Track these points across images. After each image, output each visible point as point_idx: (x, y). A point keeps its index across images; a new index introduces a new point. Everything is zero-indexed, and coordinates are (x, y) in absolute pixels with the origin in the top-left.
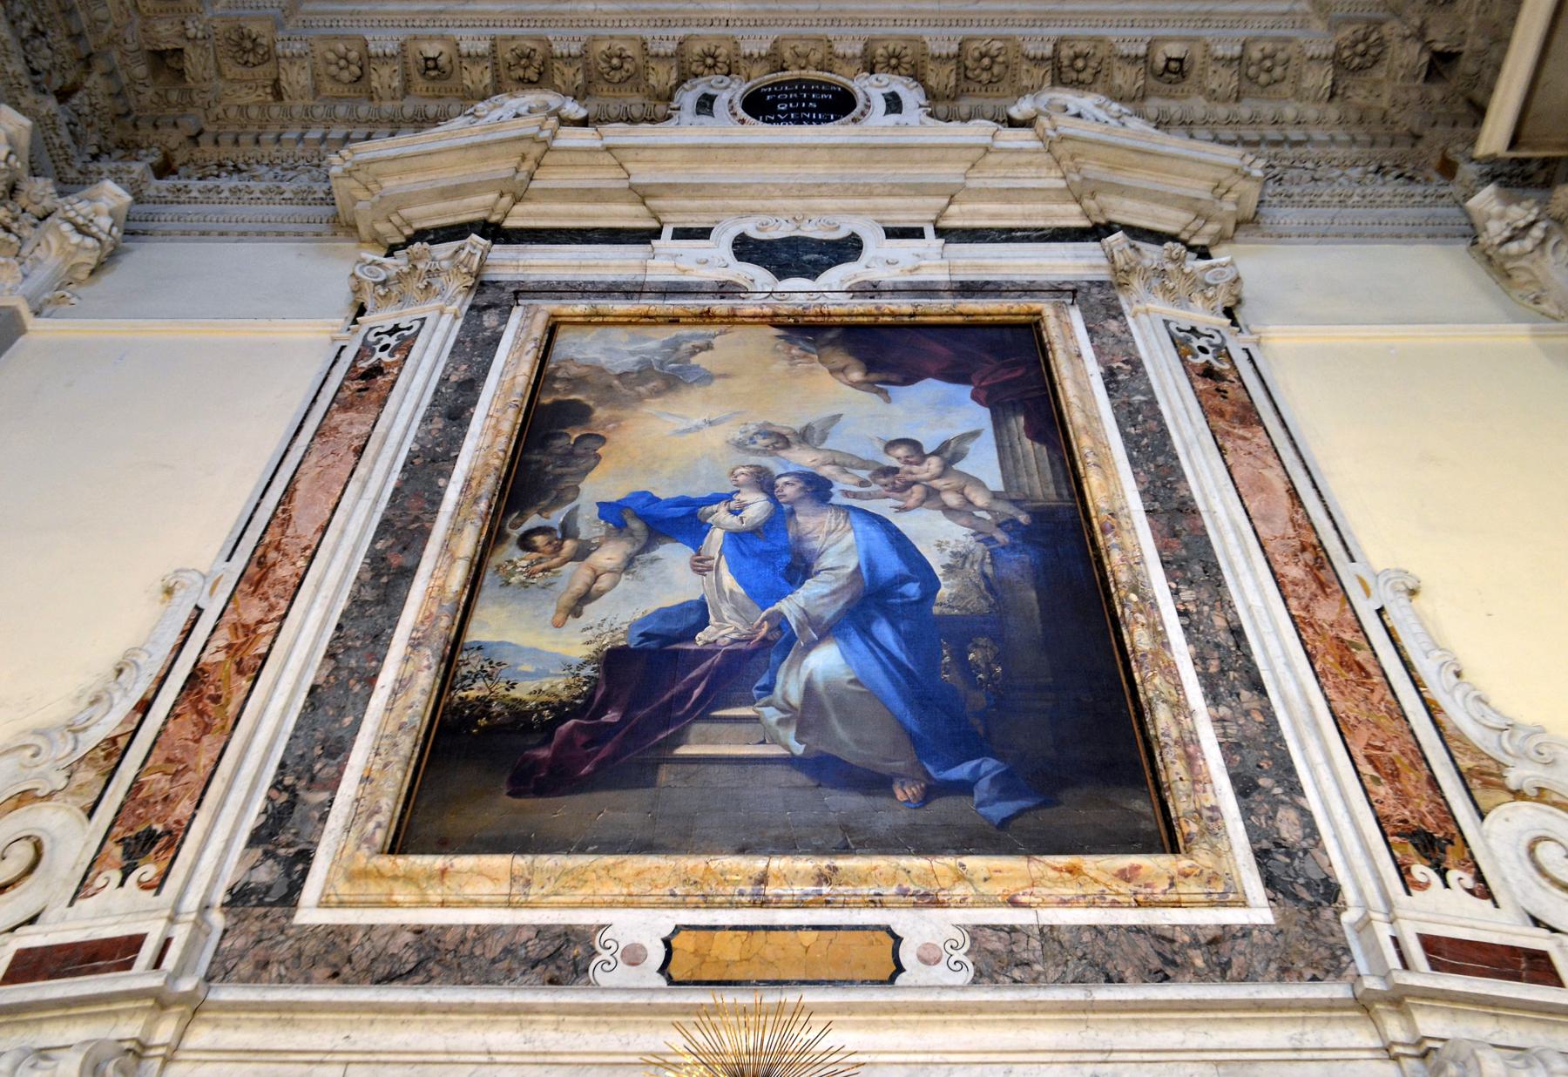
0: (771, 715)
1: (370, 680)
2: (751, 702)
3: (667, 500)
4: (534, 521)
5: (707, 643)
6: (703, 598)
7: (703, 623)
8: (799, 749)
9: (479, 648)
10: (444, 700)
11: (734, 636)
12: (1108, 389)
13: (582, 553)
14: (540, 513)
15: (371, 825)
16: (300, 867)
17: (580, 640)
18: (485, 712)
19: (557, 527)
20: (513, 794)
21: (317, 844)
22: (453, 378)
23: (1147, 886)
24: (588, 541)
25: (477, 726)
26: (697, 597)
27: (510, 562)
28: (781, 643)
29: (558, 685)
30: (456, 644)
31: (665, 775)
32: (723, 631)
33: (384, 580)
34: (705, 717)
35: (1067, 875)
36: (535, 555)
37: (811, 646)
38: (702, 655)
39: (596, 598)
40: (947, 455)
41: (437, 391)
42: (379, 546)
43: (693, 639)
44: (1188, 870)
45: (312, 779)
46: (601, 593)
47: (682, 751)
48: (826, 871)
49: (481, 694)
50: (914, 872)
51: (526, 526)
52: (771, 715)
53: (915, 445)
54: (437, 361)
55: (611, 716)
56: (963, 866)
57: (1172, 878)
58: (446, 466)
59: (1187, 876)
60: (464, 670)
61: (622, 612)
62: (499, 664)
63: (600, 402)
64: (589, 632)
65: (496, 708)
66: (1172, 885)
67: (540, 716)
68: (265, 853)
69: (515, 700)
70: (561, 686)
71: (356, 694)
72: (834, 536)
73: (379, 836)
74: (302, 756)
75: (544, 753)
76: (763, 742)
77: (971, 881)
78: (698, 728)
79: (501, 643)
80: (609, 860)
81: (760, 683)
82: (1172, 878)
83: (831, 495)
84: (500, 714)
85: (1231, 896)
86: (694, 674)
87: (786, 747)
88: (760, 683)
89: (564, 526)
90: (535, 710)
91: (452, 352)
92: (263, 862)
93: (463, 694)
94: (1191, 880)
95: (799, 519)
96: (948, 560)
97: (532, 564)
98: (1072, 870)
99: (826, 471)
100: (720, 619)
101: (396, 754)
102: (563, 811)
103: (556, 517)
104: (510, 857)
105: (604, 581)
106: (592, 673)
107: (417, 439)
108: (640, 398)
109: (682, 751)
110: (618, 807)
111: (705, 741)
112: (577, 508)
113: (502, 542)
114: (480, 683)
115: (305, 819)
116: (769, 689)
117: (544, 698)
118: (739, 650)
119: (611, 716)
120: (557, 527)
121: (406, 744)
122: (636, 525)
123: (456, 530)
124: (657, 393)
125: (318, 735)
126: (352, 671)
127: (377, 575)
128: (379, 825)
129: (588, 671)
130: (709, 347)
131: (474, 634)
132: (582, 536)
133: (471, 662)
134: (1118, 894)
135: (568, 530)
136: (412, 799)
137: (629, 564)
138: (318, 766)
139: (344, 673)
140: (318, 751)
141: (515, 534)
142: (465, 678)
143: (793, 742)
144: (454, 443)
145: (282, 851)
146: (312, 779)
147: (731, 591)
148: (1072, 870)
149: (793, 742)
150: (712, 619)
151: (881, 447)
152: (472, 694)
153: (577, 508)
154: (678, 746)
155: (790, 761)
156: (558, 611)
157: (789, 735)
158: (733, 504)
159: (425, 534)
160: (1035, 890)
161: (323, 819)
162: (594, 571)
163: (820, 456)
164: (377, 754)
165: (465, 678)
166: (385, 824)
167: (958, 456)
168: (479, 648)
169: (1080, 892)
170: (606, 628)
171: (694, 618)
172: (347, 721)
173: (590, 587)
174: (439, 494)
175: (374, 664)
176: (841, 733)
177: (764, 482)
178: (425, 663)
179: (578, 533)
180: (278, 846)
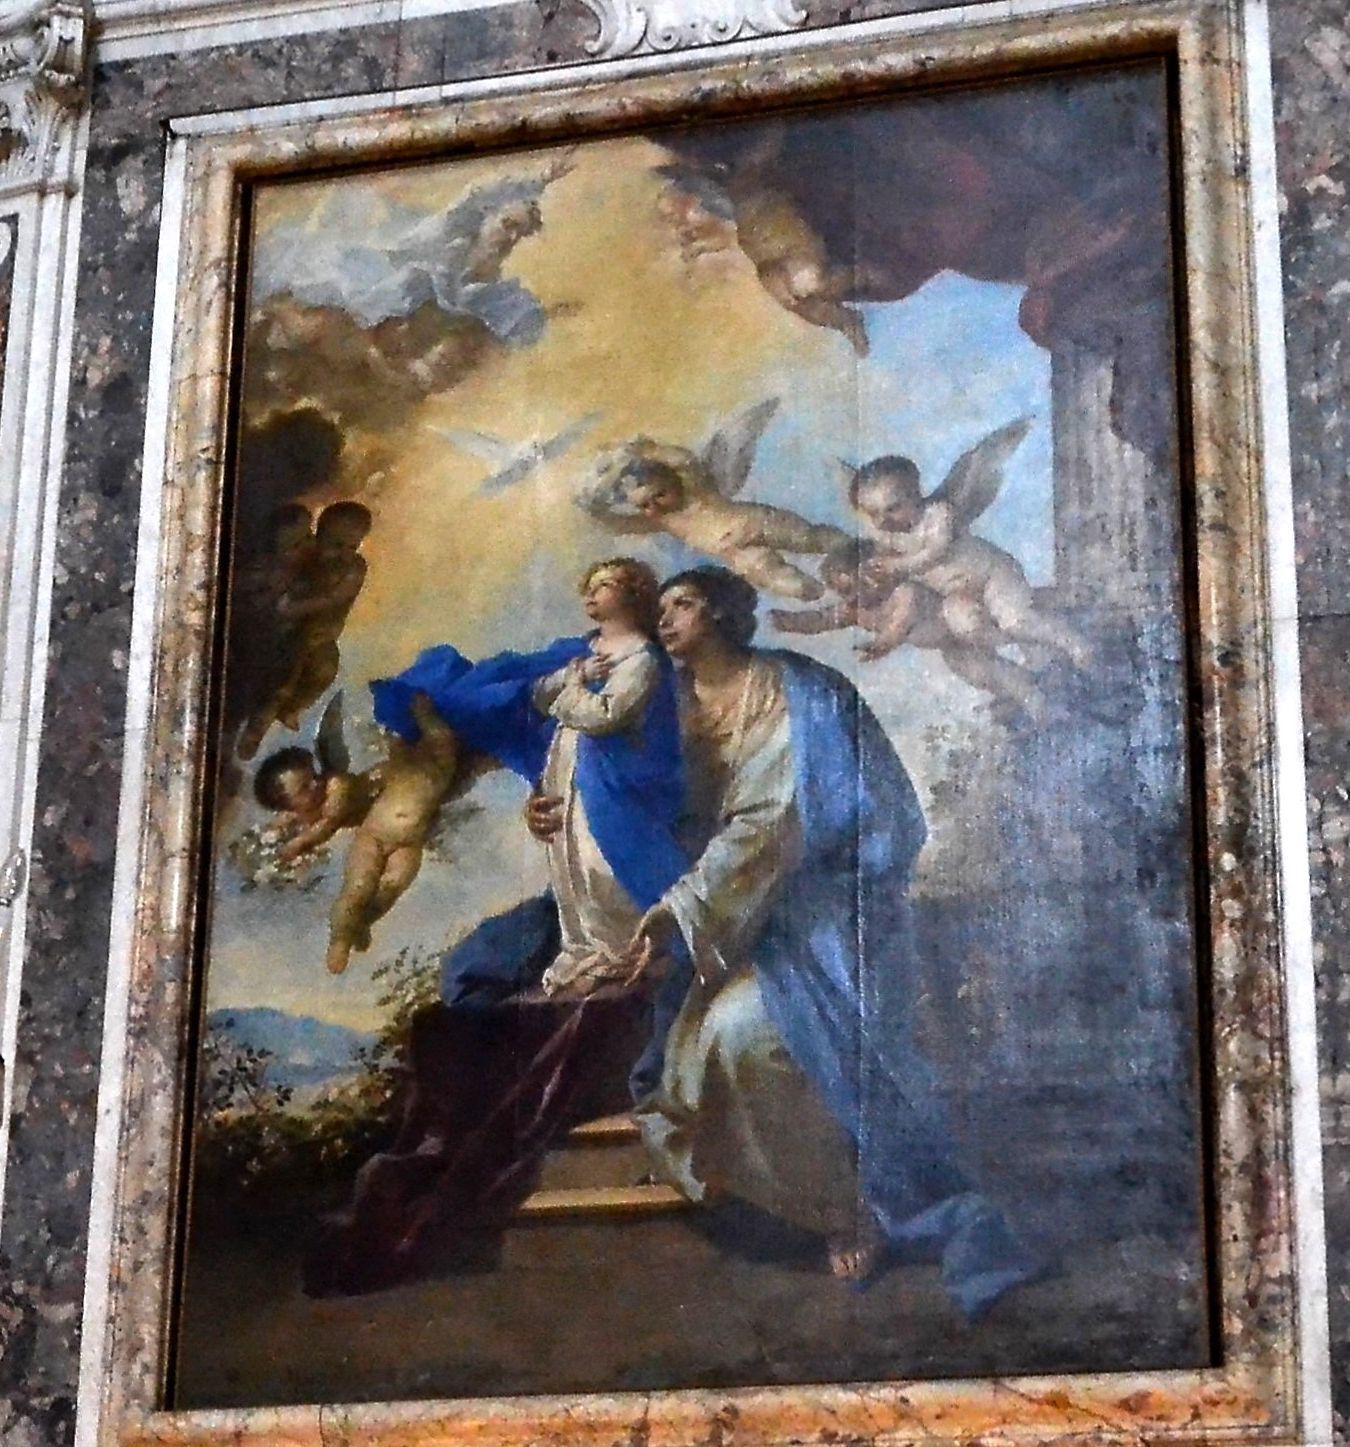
0: (657, 1128)
1: (88, 1101)
2: (622, 1106)
3: (483, 664)
4: (275, 737)
5: (560, 989)
6: (549, 893)
7: (549, 949)
8: (697, 1191)
9: (230, 1024)
10: (198, 1127)
11: (600, 971)
12: (1285, 262)
13: (356, 810)
14: (282, 718)
15: (137, 1369)
16: (62, 1426)
17: (371, 998)
18: (256, 1150)
19: (312, 748)
20: (315, 1291)
21: (76, 1388)
22: (94, 378)
23: (1160, 1418)
24: (364, 776)
25: (248, 1173)
26: (540, 892)
27: (250, 834)
28: (668, 987)
29: (347, 1086)
30: (192, 1016)
31: (513, 1248)
32: (581, 962)
33: (70, 894)
34: (568, 1143)
35: (1047, 1408)
36: (284, 817)
37: (717, 985)
38: (551, 1014)
39: (390, 903)
40: (962, 494)
41: (72, 417)
42: (49, 819)
43: (534, 983)
44: (1216, 1397)
45: (48, 1285)
46: (394, 893)
47: (535, 1203)
48: (724, 1415)
49: (244, 1113)
50: (841, 1412)
51: (263, 752)
52: (657, 1128)
53: (899, 469)
54: (56, 333)
55: (430, 1145)
56: (904, 1400)
57: (1195, 1407)
58: (114, 616)
59: (1215, 1403)
60: (214, 1069)
61: (433, 925)
62: (263, 1053)
63: (354, 414)
64: (383, 980)
65: (269, 1139)
66: (1196, 1416)
67: (332, 1152)
68: (16, 1406)
69: (292, 1121)
70: (354, 1092)
71: (75, 1130)
72: (759, 730)
73: (150, 1384)
74: (25, 1244)
75: (344, 1219)
76: (645, 1181)
77: (920, 1421)
78: (554, 1161)
79: (261, 1012)
80: (440, 1408)
81: (637, 1068)
82: (1195, 1407)
83: (752, 627)
84: (276, 1150)
85: (1277, 1430)
86: (540, 1057)
87: (679, 1188)
88: (637, 1068)
89: (323, 743)
90: (323, 1140)
91: (79, 302)
92: (16, 1421)
93: (219, 1115)
94: (1219, 1409)
95: (701, 691)
96: (943, 773)
97: (283, 839)
98: (1058, 1402)
99: (746, 563)
100: (578, 937)
101: (146, 1248)
102: (374, 1322)
103: (309, 727)
104: (315, 1408)
105: (398, 861)
106: (395, 1063)
107: (62, 554)
108: (417, 395)
109: (535, 1203)
110: (447, 1313)
111: (566, 1184)
112: (339, 695)
113: (233, 794)
114: (240, 1094)
115: (53, 1350)
116: (651, 1078)
117: (332, 1115)
118: (605, 1002)
119: (430, 1145)
120: (312, 748)
121: (156, 1226)
122: (436, 732)
123: (158, 784)
124: (449, 375)
125: (40, 1205)
126: (60, 1084)
127: (58, 886)
128: (146, 1368)
129: (388, 1060)
130: (532, 223)
131: (222, 996)
132: (355, 766)
133: (222, 1053)
134: (1120, 1431)
135: (331, 752)
136: (174, 1346)
137: (431, 826)
138: (50, 1260)
139: (49, 1089)
140: (45, 1235)
141: (249, 768)
142: (218, 1084)
143: (687, 1178)
144: (120, 551)
145: (35, 1402)
146: (48, 1285)
147: (593, 872)
148: (1058, 1402)
149: (687, 1178)
150: (565, 936)
151: (841, 481)
152: (232, 1114)
153: (339, 695)
154: (526, 1195)
155: (683, 1212)
156: (334, 940)
157: (683, 1166)
158: (590, 665)
159: (112, 781)
160: (1006, 1429)
161: (75, 1347)
162: (380, 844)
163: (736, 524)
164: (123, 1240)
165: (218, 1084)
166: (153, 1365)
167: (980, 500)
168: (230, 1024)
169: (1068, 1429)
170: (406, 970)
171: (532, 942)
172: (72, 1177)
173: (376, 880)
174: (117, 691)
175: (87, 1067)
176: (757, 1158)
177: (637, 600)
178: (157, 1079)
179: (346, 760)
180: (28, 1395)
